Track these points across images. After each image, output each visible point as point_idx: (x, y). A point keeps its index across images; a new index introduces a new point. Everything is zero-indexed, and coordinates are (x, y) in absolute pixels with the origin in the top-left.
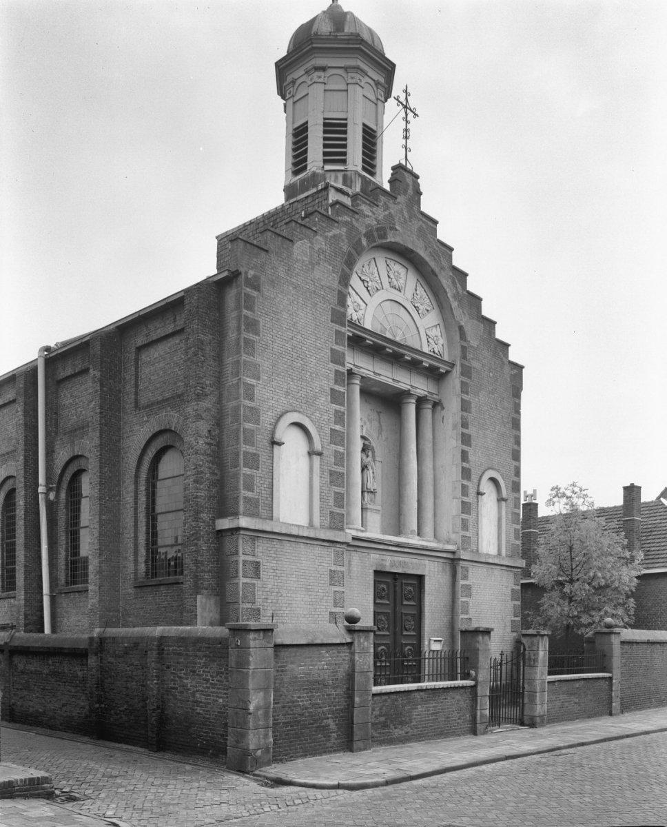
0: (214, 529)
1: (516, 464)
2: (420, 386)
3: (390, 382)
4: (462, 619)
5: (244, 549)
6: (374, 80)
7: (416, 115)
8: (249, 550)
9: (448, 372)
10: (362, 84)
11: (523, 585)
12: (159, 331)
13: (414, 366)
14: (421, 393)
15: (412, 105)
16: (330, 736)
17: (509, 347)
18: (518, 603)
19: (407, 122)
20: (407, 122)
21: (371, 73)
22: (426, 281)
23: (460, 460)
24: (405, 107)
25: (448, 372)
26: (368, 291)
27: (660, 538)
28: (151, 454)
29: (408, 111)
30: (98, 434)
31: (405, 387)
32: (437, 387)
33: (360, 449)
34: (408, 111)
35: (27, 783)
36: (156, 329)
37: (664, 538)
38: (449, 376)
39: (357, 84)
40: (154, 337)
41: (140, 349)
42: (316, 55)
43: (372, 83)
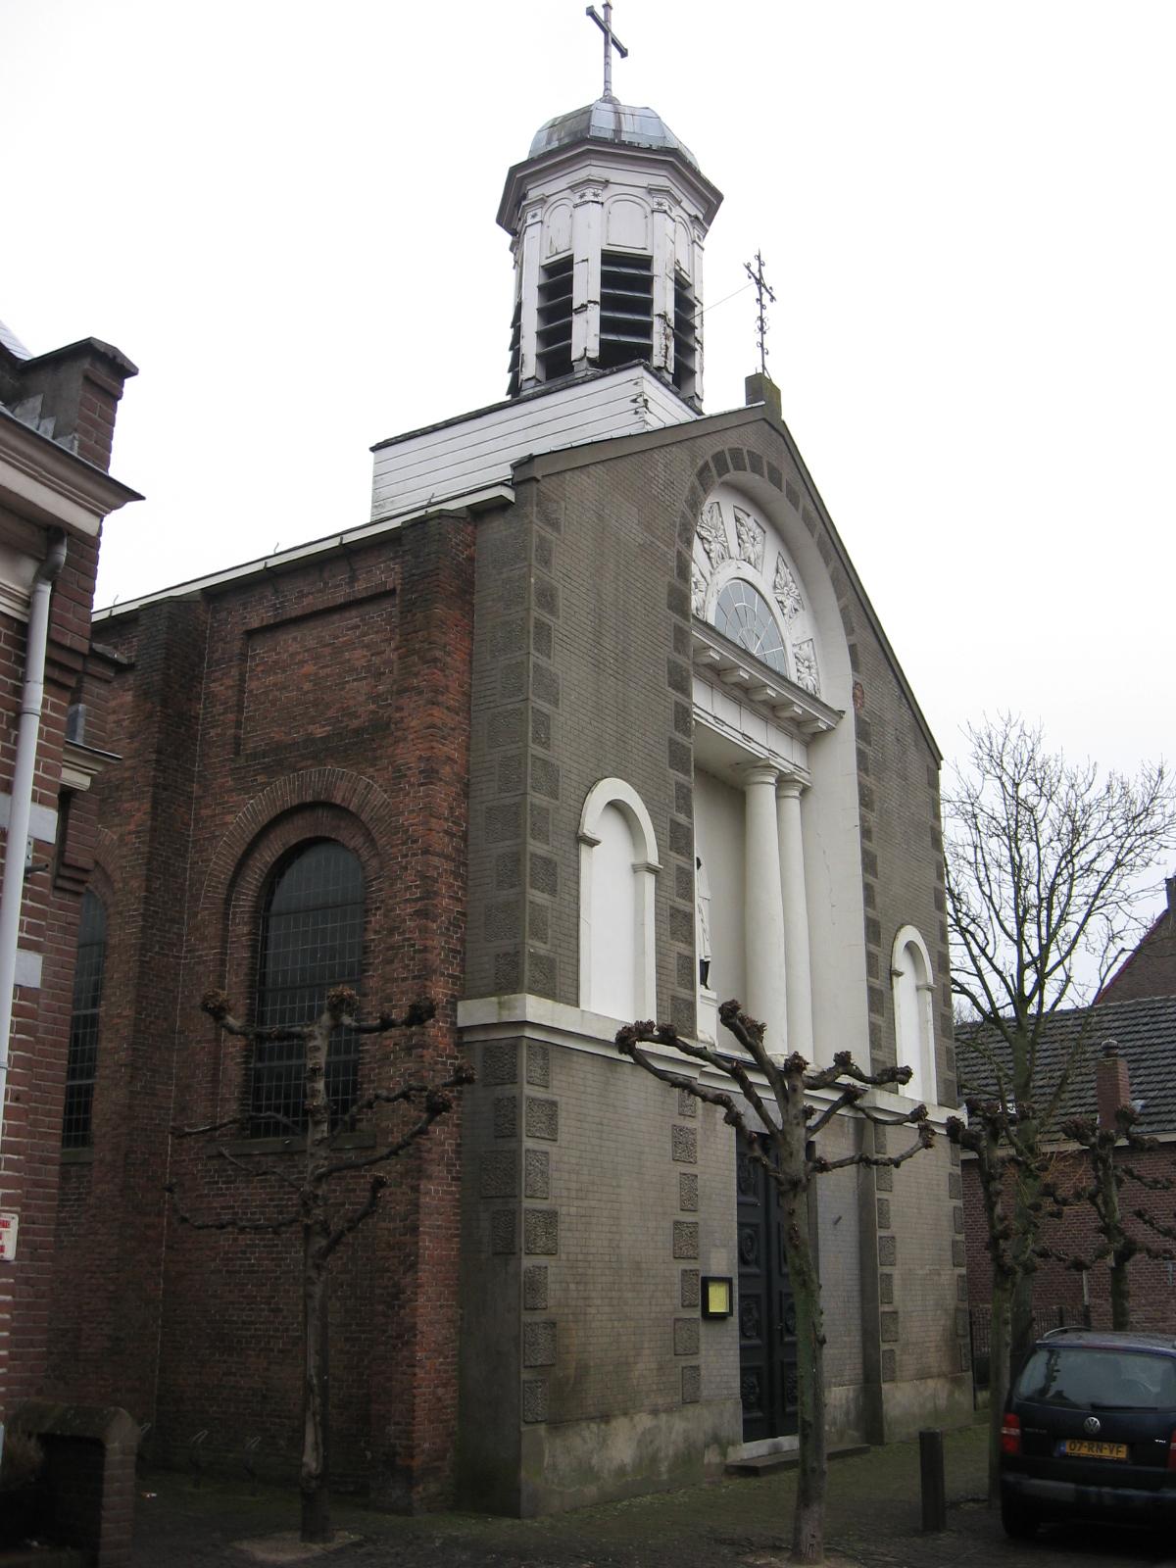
0: (455, 1023)
1: (872, 913)
2: (784, 752)
3: (737, 739)
4: (881, 1238)
5: (529, 1071)
6: (689, 215)
7: (773, 298)
8: (537, 1073)
9: (823, 732)
10: (673, 215)
11: (965, 1162)
12: (305, 602)
13: (772, 712)
14: (787, 768)
15: (767, 281)
16: (911, 1317)
17: (128, 382)
18: (959, 1203)
19: (763, 307)
20: (763, 307)
21: (686, 204)
22: (798, 568)
23: (862, 902)
24: (759, 282)
25: (830, 729)
26: (709, 558)
27: (1160, 1074)
28: (269, 854)
29: (763, 290)
30: (147, 806)
31: (763, 753)
32: (805, 749)
33: (26, 843)
34: (763, 290)
35: (973, 1155)
36: (302, 595)
37: (1169, 1073)
38: (834, 732)
39: (665, 212)
40: (294, 610)
41: (251, 634)
42: (594, 162)
43: (685, 216)
